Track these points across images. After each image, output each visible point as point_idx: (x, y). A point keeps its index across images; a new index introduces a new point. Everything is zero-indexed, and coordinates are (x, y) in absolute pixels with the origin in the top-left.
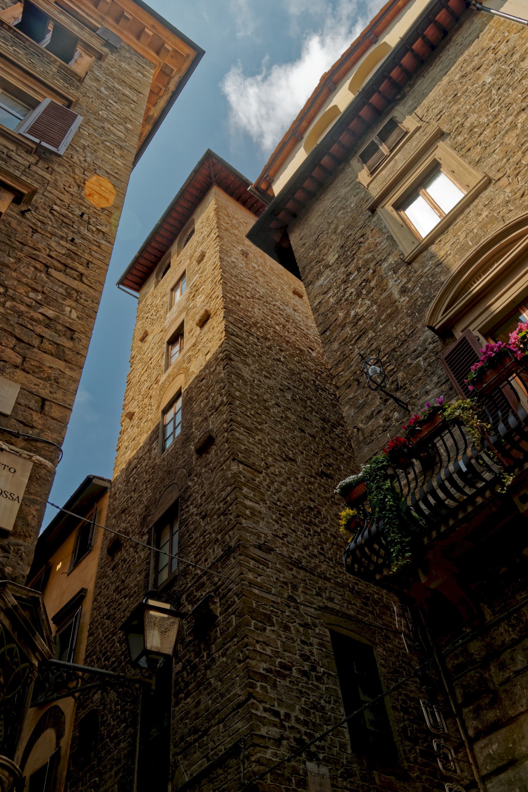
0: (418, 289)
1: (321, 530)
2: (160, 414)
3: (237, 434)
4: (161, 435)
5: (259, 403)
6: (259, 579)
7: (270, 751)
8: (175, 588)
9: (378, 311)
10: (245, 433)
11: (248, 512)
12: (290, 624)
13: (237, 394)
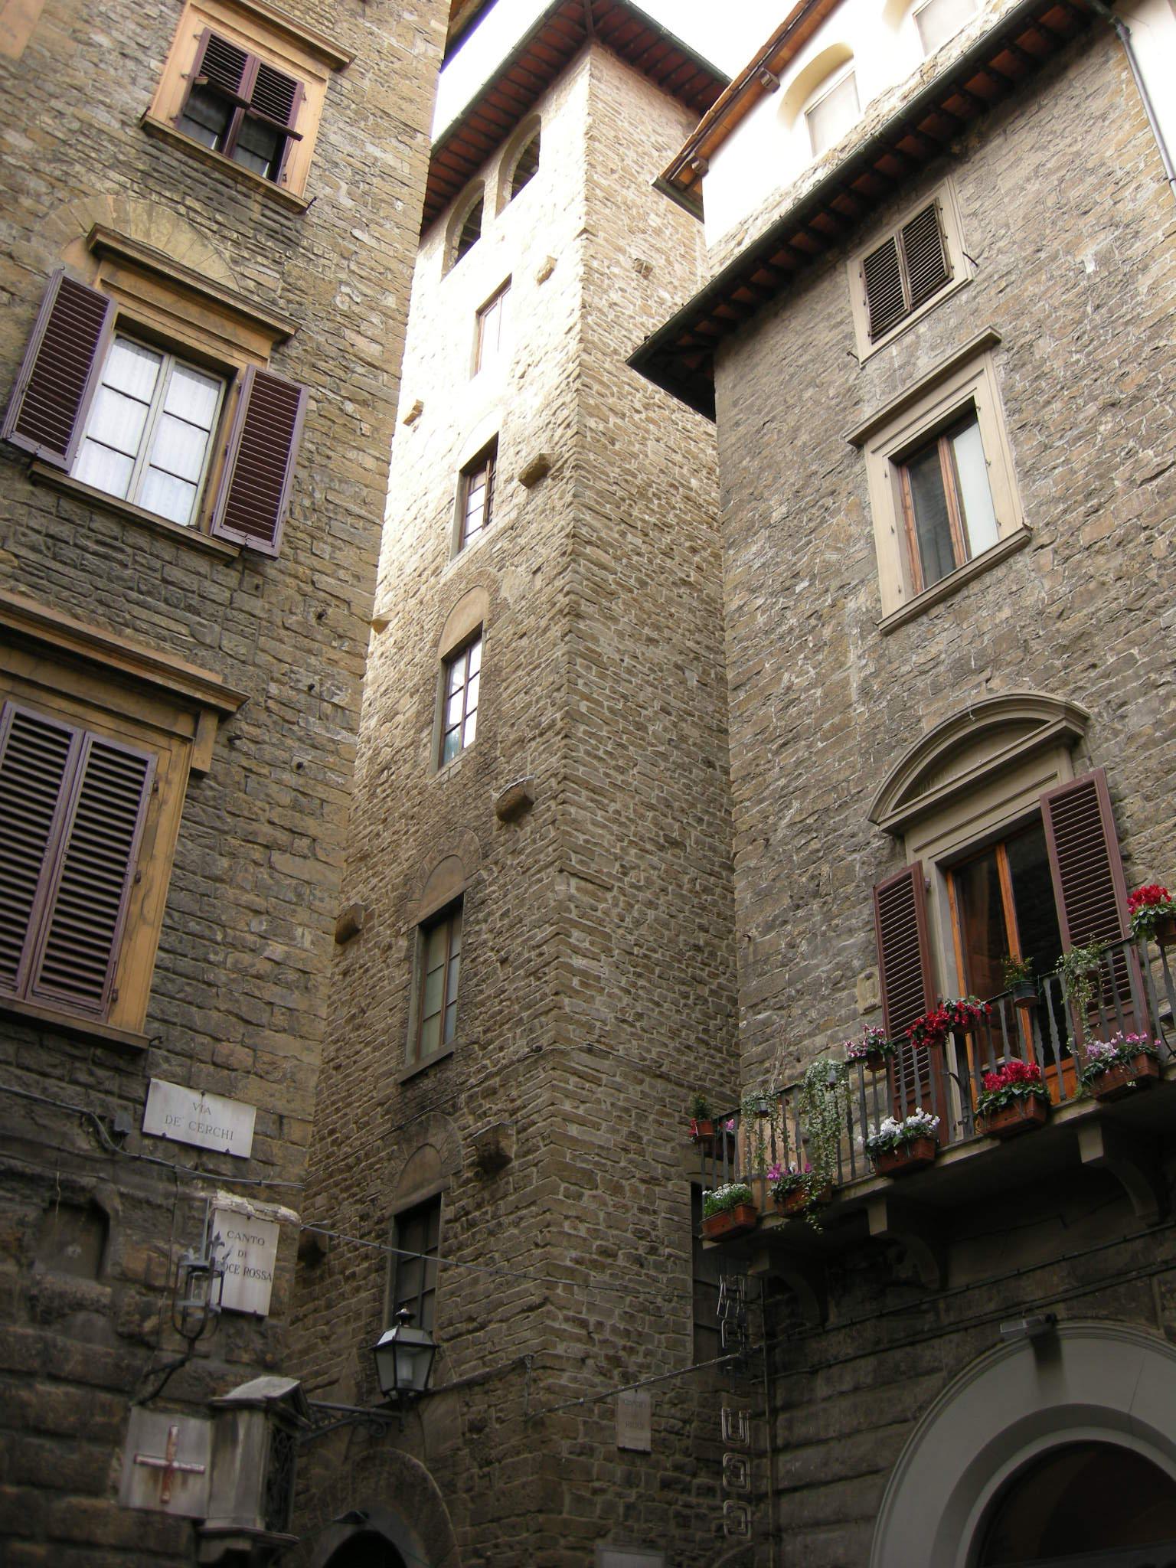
0: (885, 704)
1: (711, 991)
2: (438, 666)
3: (573, 810)
4: (437, 718)
5: (625, 719)
6: (580, 1112)
7: (566, 1375)
8: (449, 1073)
9: (824, 704)
10: (589, 804)
11: (575, 982)
12: (623, 1182)
13: (583, 707)
